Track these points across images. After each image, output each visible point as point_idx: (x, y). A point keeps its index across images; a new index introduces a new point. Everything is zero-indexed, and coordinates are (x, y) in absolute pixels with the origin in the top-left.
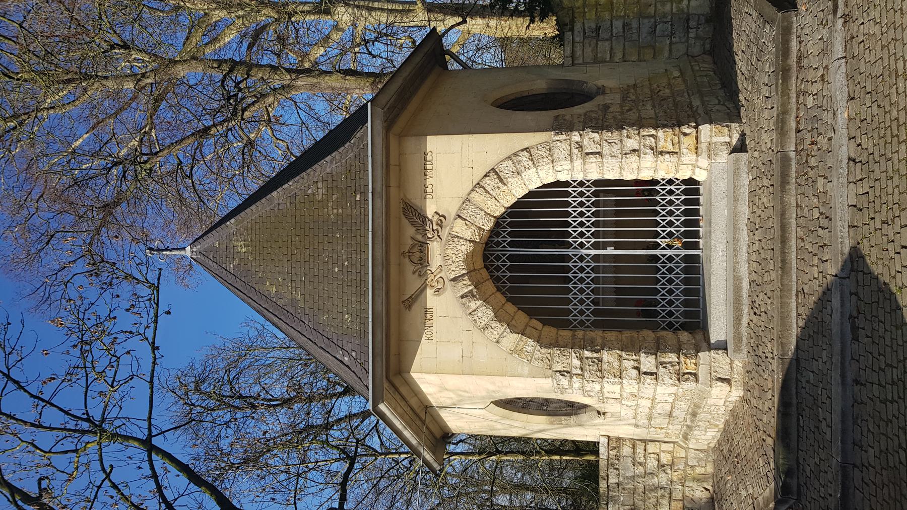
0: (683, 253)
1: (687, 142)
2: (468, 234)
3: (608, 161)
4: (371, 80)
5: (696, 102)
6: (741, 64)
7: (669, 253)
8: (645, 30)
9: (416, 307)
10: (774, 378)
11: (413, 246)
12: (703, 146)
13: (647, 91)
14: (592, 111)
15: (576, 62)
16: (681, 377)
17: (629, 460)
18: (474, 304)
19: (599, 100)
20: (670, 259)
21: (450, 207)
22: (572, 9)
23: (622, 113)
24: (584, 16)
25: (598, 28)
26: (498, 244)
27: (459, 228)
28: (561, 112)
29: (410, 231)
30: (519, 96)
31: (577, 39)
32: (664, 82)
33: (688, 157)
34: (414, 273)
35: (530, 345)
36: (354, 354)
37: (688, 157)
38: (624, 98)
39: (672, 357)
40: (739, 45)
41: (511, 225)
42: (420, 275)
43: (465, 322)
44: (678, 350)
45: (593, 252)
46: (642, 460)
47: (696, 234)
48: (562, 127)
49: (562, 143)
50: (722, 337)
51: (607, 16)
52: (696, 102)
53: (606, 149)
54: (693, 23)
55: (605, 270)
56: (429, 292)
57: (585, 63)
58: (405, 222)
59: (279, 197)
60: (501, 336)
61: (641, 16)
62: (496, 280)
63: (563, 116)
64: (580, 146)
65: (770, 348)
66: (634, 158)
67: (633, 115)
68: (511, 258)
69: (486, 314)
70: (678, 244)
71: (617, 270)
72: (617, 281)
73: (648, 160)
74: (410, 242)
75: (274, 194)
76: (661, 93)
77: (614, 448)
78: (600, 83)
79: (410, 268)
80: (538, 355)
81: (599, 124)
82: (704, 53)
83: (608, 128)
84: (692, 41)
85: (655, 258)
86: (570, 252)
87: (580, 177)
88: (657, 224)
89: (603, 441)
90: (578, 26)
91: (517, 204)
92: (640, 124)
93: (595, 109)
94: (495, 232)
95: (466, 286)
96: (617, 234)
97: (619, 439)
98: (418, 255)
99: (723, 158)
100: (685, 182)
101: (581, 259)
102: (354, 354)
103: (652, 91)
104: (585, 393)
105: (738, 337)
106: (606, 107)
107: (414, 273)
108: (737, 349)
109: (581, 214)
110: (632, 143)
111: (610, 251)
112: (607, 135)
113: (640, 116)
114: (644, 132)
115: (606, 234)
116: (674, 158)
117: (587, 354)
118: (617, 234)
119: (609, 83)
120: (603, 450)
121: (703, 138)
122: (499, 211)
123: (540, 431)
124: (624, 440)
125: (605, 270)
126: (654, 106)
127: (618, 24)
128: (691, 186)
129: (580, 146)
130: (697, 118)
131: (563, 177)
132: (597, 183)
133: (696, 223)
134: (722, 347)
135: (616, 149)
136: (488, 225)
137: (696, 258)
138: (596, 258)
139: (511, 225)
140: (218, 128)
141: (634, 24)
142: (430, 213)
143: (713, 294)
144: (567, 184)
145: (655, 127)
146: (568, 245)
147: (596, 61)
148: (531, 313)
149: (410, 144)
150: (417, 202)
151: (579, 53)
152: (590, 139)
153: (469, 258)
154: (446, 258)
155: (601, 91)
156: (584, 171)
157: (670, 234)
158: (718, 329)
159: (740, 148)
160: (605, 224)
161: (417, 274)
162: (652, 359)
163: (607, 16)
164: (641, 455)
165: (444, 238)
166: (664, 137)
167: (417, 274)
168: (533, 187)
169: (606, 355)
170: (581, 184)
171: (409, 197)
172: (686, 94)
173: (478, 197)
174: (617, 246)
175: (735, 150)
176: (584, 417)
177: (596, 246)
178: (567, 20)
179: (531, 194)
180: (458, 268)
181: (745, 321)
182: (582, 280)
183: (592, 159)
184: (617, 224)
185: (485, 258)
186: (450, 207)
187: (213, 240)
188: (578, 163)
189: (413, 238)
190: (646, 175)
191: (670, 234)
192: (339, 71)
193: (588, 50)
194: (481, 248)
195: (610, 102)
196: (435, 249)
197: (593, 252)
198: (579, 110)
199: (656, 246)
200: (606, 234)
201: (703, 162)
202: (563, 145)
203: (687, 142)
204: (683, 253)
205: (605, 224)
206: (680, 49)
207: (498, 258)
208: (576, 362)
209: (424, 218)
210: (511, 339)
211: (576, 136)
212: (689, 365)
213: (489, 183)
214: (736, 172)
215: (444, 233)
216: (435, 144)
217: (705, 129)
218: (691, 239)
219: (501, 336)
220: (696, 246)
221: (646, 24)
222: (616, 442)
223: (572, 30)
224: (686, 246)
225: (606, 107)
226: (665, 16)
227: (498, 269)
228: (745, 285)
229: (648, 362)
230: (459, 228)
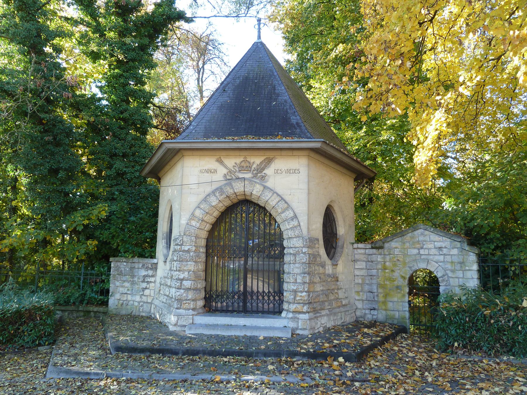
11: (249, 163)
13: (333, 287)
14: (320, 258)
15: (355, 250)
23: (319, 274)
24: (379, 254)
28: (321, 242)
30: (336, 220)
31: (367, 251)
34: (236, 163)
36: (194, 131)
42: (234, 166)
46: (146, 280)
58: (265, 157)
63: (318, 244)
69: (214, 201)
74: (252, 161)
76: (331, 294)
77: (152, 266)
82: (357, 318)
84: (364, 311)
89: (155, 261)
93: (322, 260)
97: (156, 269)
98: (245, 166)
102: (194, 131)
103: (333, 289)
107: (236, 163)
113: (316, 283)
119: (340, 268)
126: (322, 290)
140: (205, 44)
143: (256, 319)
161: (235, 165)
164: (148, 280)
167: (235, 165)
172: (329, 307)
176: (165, 251)
189: (254, 163)
195: (327, 268)
222: (155, 267)
225: (323, 266)
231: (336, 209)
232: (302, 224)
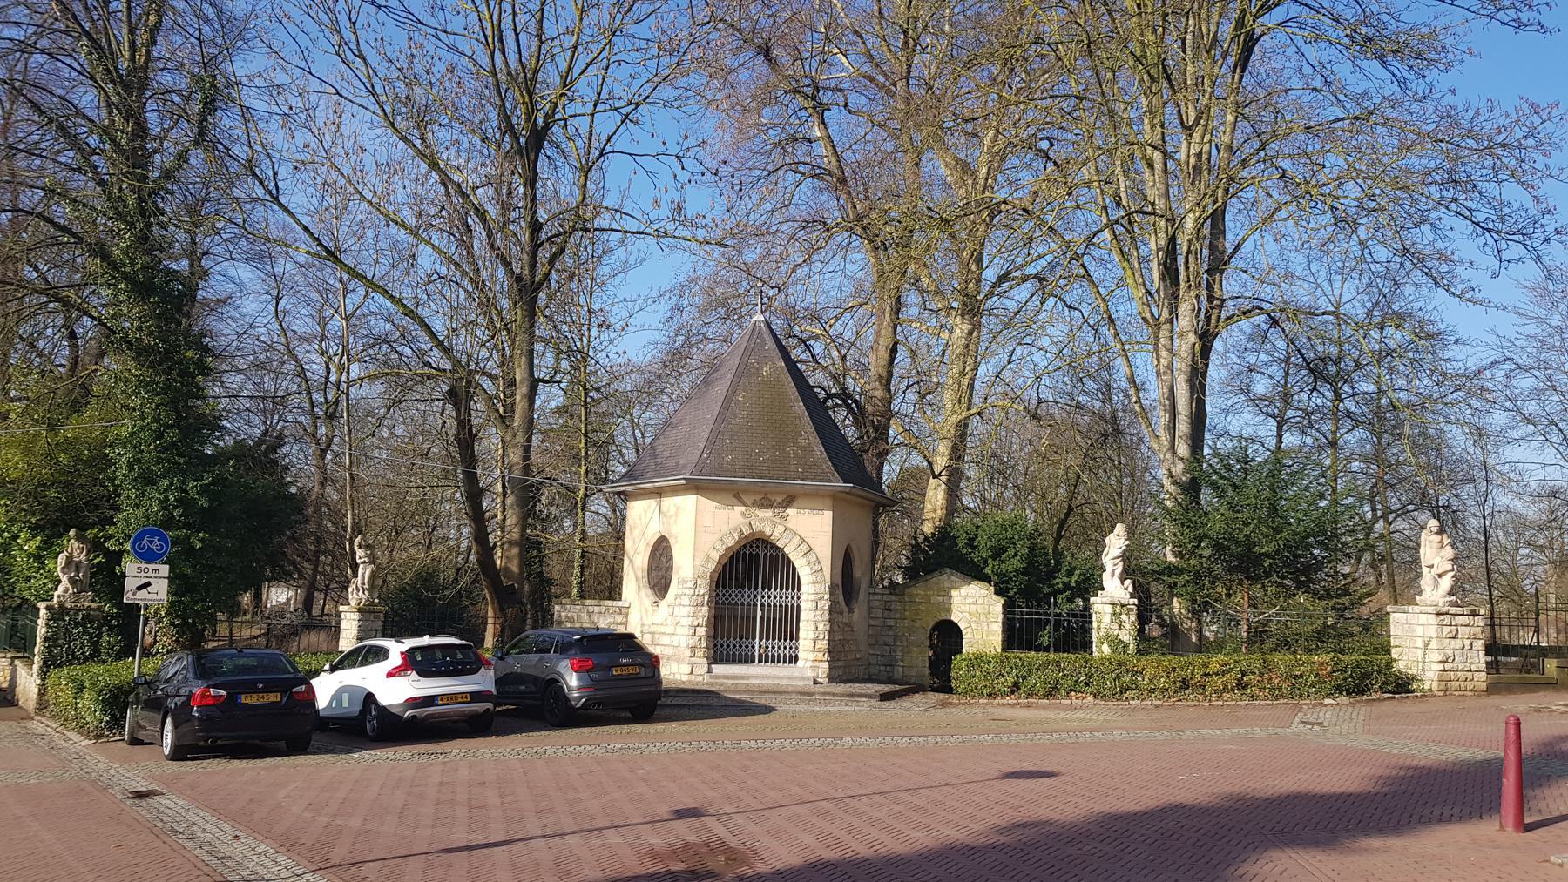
0: (757, 654)
1: (820, 656)
2: (776, 533)
3: (813, 613)
4: (884, 374)
5: (840, 663)
6: (862, 685)
7: (757, 647)
8: (886, 639)
9: (735, 500)
10: (705, 687)
12: (817, 664)
13: (849, 637)
16: (693, 648)
17: (612, 620)
18: (736, 535)
19: (846, 609)
20: (753, 647)
21: (791, 524)
22: (904, 594)
25: (890, 610)
26: (766, 547)
27: (780, 528)
28: (841, 588)
29: (779, 499)
32: (853, 648)
33: (812, 656)
35: (712, 566)
37: (812, 656)
38: (846, 624)
39: (704, 645)
40: (870, 685)
41: (777, 555)
43: (725, 529)
44: (707, 647)
45: (759, 603)
47: (766, 662)
48: (833, 589)
49: (824, 589)
50: (714, 671)
51: (897, 616)
52: (840, 663)
53: (818, 612)
54: (888, 668)
55: (748, 610)
56: (743, 508)
57: (86, 659)
59: (799, 407)
60: (717, 550)
61: (896, 637)
62: (745, 546)
64: (821, 599)
65: (722, 688)
66: (813, 627)
67: (836, 628)
68: (757, 555)
69: (730, 542)
70: (762, 651)
71: (748, 617)
72: (729, 617)
73: (812, 635)
75: (801, 404)
78: (856, 610)
79: (758, 498)
80: (706, 570)
81: (833, 610)
83: (830, 614)
85: (754, 639)
86: (760, 589)
87: (802, 597)
88: (773, 640)
90: (893, 598)
91: (789, 561)
92: (831, 632)
94: (774, 546)
95: (746, 531)
96: (768, 619)
97: (627, 614)
99: (811, 674)
100: (796, 657)
101: (755, 596)
104: (677, 596)
105: (718, 677)
106: (841, 614)
108: (711, 677)
109: (781, 597)
110: (821, 627)
111: (759, 613)
112: (827, 613)
114: (827, 633)
115: (769, 611)
116: (811, 649)
117: (706, 598)
118: (768, 619)
119: (856, 615)
120: (620, 603)
121: (821, 664)
122: (786, 551)
123: (631, 561)
124: (627, 617)
125: (748, 610)
127: (892, 623)
128: (794, 659)
129: (821, 599)
130: (832, 661)
131: (804, 589)
132: (799, 606)
133: (773, 662)
134: (710, 671)
135: (819, 618)
136: (779, 544)
137: (753, 661)
138: (755, 605)
139: (777, 555)
141: (891, 633)
142: (789, 511)
144: (799, 590)
145: (829, 640)
146: (763, 589)
147: (871, 608)
148: (725, 566)
149: (829, 502)
150: (795, 504)
151: (876, 597)
152: (825, 604)
153: (762, 533)
154: (763, 520)
155: (851, 611)
156: (807, 600)
157: (767, 647)
158: (719, 669)
159: (815, 682)
160: (775, 611)
162: (704, 633)
163: (897, 616)
165: (775, 519)
166: (823, 644)
168: (798, 570)
169: (705, 608)
170: (799, 598)
171: (799, 500)
173: (797, 540)
174: (762, 618)
175: (814, 680)
177: (762, 605)
178: (897, 591)
179: (794, 569)
180: (757, 527)
181: (726, 681)
182: (743, 596)
183: (814, 605)
184: (774, 619)
185: (758, 540)
186: (791, 524)
187: (770, 344)
188: (812, 597)
190: (802, 634)
191: (767, 647)
192: (895, 345)
193: (877, 603)
194: (766, 538)
196: (767, 513)
197: (759, 603)
198: (841, 598)
199: (761, 639)
200: (769, 611)
201: (809, 664)
202: (822, 589)
203: (820, 656)
204: (757, 654)
205: (775, 611)
206: (873, 661)
207: (758, 547)
208: (702, 592)
209: (786, 508)
210: (716, 556)
211: (827, 596)
212: (700, 653)
213: (804, 548)
214: (803, 679)
215: (777, 519)
216: (828, 516)
217: (826, 665)
218: (766, 659)
219: (717, 550)
220: (760, 661)
221: (890, 641)
223: (891, 594)
224: (760, 655)
225: (841, 614)
226: (895, 652)
227: (751, 547)
228: (747, 682)
229: (702, 631)
230: (780, 528)
231: (854, 548)
232: (824, 569)
